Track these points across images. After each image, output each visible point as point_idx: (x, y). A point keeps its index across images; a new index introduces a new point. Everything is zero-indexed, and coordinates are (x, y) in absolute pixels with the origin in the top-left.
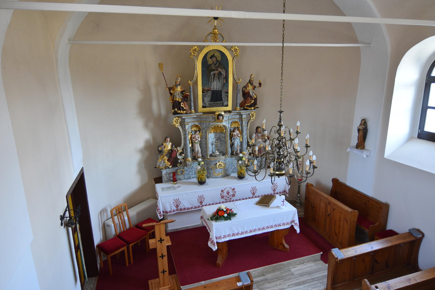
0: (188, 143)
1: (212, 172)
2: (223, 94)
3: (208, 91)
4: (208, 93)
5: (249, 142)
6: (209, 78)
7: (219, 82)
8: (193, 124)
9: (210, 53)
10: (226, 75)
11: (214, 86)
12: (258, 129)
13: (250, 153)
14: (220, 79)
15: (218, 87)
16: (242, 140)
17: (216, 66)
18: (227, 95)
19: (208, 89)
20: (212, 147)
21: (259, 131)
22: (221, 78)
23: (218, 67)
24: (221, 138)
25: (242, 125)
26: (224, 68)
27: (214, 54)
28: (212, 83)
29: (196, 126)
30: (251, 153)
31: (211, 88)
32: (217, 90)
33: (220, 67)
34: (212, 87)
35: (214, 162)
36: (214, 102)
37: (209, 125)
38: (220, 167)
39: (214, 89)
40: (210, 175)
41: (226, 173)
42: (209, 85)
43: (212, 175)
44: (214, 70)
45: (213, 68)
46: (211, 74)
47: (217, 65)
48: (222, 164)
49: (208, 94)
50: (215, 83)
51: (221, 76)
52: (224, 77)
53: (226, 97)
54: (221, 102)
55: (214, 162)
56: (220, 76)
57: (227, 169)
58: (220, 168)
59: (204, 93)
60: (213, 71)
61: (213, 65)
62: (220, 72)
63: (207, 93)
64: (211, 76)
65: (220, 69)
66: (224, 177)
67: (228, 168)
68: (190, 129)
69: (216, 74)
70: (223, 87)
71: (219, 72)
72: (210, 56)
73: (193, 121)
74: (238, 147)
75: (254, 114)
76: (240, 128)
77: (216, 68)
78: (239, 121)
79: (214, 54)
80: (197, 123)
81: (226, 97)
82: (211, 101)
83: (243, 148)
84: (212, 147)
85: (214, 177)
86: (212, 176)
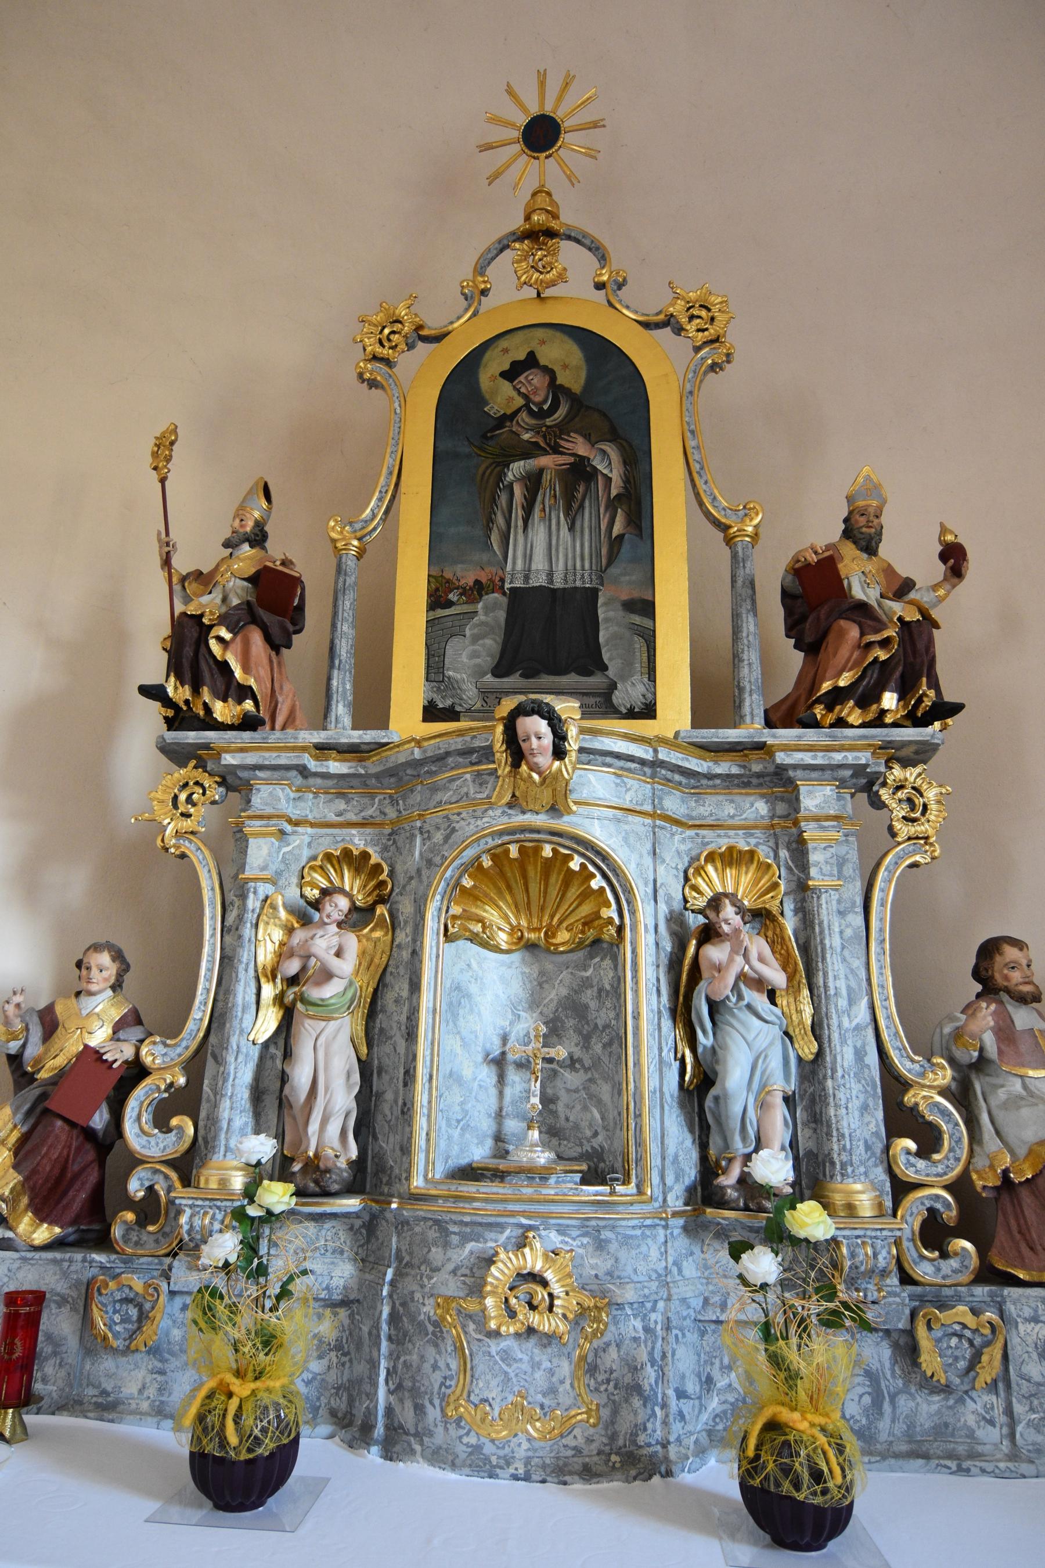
0: (239, 1000)
1: (437, 1378)
2: (611, 614)
3: (481, 596)
4: (480, 605)
5: (905, 1085)
6: (494, 501)
7: (571, 528)
8: (331, 842)
9: (506, 351)
10: (627, 480)
11: (529, 558)
12: (998, 958)
13: (931, 1211)
14: (581, 506)
15: (560, 567)
16: (818, 1038)
17: (549, 422)
18: (646, 622)
19: (477, 582)
20: (501, 1094)
21: (1016, 976)
22: (587, 503)
23: (563, 428)
24: (586, 1007)
25: (802, 889)
26: (614, 436)
27: (531, 355)
28: (518, 542)
29: (357, 862)
30: (950, 1215)
31: (503, 569)
32: (558, 583)
33: (576, 432)
34: (514, 563)
35: (465, 1239)
36: (525, 676)
37: (447, 838)
38: (535, 1319)
39: (527, 578)
40: (419, 1409)
41: (624, 1426)
42: (489, 547)
43: (433, 1413)
44: (529, 451)
45: (526, 436)
46: (510, 476)
47: (556, 416)
48: (549, 1275)
49: (481, 617)
50: (539, 534)
51: (587, 489)
52: (614, 492)
53: (639, 643)
54: (596, 681)
55: (471, 1246)
56: (581, 489)
57: (635, 1369)
58: (531, 1331)
59: (450, 604)
60: (526, 456)
61: (527, 420)
62: (582, 458)
63: (466, 608)
64: (510, 488)
65: (580, 440)
66: (588, 1474)
67: (643, 1356)
68: (295, 880)
69: (546, 477)
70: (610, 562)
71: (572, 459)
72: (506, 366)
73: (332, 817)
74: (763, 1105)
75: (931, 794)
76: (789, 924)
77: (544, 437)
78: (776, 856)
79: (531, 355)
80: (358, 841)
81: (636, 638)
82: (499, 671)
83: (829, 1134)
84: (501, 1094)
85: (461, 1450)
86: (439, 1437)
